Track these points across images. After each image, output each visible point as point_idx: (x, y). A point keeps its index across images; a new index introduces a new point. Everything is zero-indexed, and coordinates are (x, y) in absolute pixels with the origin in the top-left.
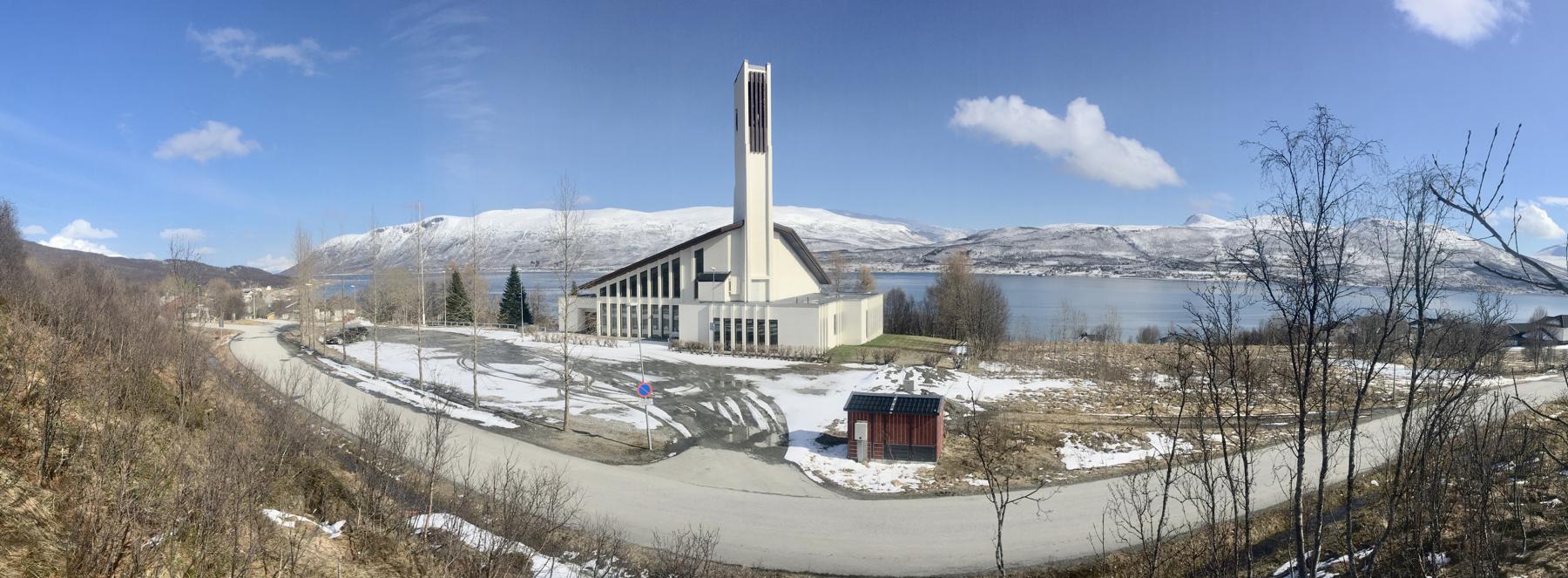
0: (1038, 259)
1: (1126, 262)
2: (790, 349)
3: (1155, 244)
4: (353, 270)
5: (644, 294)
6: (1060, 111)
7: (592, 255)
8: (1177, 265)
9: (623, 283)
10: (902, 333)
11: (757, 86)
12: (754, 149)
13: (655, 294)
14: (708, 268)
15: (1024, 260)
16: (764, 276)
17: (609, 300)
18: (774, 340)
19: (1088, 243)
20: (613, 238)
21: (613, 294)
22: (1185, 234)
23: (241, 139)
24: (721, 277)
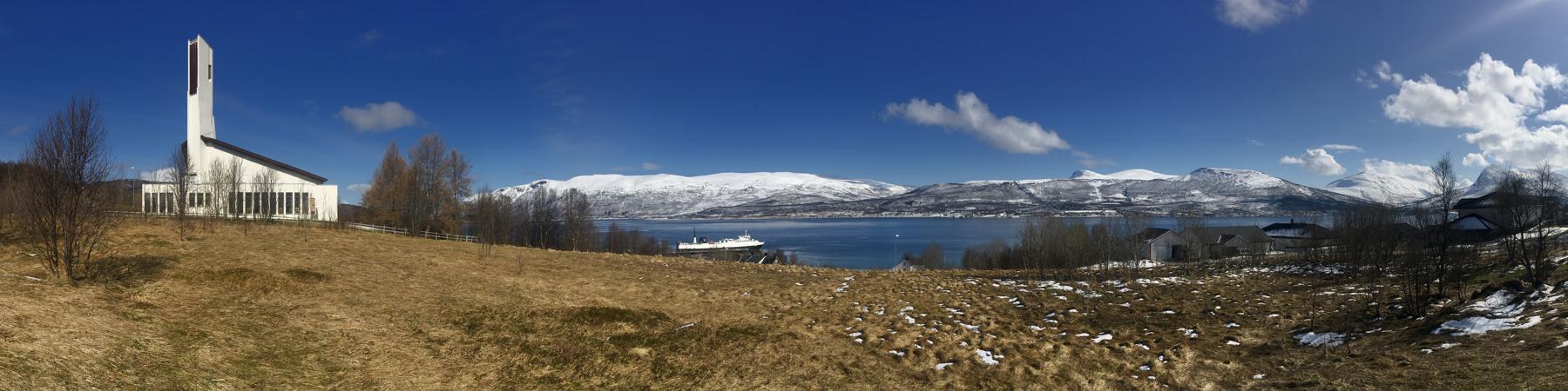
1: (1023, 205)
3: (1046, 192)
4: (818, 210)
6: (951, 104)
7: (648, 207)
10: (534, 243)
15: (951, 207)
20: (664, 195)
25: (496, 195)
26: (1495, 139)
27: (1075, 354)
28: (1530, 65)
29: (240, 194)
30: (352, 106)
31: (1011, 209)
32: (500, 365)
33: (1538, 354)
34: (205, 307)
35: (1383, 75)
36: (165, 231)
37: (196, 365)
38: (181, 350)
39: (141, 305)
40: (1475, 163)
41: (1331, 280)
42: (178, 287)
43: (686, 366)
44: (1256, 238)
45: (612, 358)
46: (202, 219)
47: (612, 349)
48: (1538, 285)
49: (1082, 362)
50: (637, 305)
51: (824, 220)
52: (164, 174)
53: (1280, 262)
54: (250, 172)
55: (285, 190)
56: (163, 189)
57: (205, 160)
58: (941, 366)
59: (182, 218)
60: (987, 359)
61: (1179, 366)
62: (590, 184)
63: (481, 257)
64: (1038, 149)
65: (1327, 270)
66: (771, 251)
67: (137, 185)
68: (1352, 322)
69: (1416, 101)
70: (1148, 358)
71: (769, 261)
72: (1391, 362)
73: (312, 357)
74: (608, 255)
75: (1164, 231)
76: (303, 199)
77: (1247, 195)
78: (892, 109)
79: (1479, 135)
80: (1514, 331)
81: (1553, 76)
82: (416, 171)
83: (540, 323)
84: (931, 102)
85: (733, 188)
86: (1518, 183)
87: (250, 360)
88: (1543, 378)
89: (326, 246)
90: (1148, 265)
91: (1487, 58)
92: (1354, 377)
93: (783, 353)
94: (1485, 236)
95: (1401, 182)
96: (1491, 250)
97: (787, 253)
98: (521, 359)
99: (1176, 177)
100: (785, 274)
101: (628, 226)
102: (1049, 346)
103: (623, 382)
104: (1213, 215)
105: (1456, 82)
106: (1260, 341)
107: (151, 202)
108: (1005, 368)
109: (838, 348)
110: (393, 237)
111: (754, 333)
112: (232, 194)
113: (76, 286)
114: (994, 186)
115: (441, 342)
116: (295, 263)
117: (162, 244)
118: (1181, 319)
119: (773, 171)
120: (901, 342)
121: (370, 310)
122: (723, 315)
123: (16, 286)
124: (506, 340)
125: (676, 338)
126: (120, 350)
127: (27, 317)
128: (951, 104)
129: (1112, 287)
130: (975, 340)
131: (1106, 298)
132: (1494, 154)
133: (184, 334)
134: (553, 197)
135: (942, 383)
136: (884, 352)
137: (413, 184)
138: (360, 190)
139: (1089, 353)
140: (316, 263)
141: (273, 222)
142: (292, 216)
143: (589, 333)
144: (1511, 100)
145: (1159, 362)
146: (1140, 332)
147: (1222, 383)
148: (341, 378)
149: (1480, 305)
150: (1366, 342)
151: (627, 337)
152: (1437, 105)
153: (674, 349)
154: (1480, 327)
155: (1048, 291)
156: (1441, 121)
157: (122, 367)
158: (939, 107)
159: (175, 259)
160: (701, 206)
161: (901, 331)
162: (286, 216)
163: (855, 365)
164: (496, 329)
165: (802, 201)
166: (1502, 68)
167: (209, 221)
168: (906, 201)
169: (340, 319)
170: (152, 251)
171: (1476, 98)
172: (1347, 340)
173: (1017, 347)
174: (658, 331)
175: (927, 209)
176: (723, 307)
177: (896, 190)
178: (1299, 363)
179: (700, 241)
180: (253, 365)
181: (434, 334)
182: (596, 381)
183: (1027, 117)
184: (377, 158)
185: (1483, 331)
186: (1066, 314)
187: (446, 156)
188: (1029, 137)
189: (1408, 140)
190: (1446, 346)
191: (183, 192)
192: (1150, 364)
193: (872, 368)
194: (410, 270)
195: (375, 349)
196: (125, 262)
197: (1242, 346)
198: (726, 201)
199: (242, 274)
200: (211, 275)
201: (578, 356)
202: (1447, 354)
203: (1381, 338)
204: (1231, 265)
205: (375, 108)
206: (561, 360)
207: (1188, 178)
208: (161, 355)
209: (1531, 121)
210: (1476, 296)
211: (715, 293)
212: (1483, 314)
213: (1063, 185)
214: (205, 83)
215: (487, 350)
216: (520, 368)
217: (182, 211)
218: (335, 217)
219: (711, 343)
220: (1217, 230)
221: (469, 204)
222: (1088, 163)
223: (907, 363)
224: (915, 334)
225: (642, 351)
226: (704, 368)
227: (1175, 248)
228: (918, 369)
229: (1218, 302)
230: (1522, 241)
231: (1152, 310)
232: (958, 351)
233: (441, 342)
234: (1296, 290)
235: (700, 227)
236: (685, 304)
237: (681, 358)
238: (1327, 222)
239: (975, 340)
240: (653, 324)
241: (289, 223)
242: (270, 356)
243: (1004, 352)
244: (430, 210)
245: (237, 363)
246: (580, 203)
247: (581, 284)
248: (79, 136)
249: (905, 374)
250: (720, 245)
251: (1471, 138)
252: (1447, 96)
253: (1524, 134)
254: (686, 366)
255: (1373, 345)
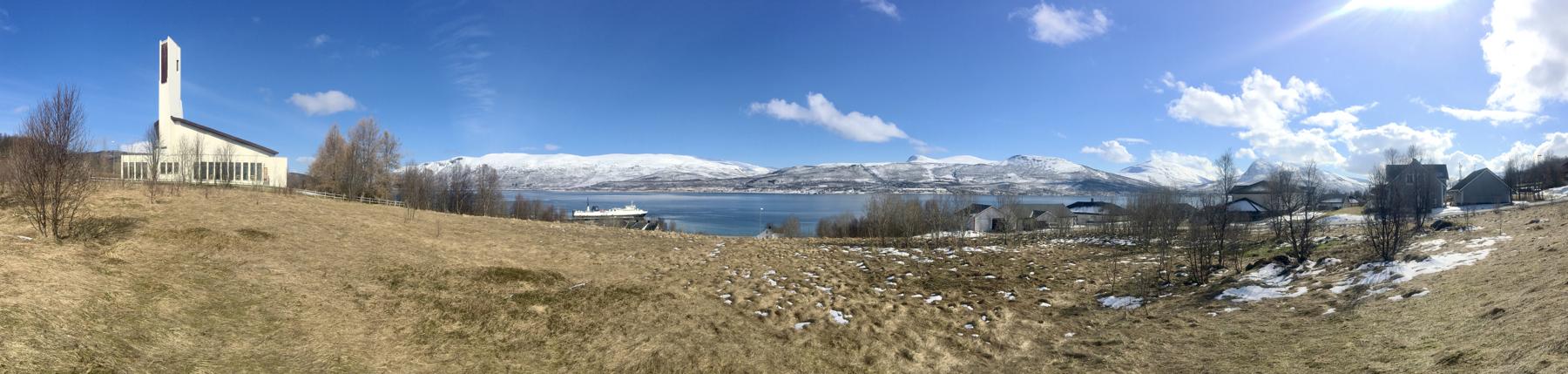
0: (816, 184)
3: (887, 173)
6: (804, 104)
8: (901, 185)
10: (452, 209)
19: (846, 174)
20: (562, 171)
22: (908, 166)
25: (421, 168)
26: (1263, 137)
27: (911, 313)
28: (1293, 80)
29: (203, 164)
30: (302, 93)
31: (857, 187)
32: (416, 320)
33: (1307, 319)
34: (168, 263)
35: (1169, 84)
36: (139, 194)
37: (156, 315)
38: (143, 301)
39: (113, 261)
40: (1246, 156)
41: (1125, 251)
42: (147, 244)
43: (577, 323)
44: (1063, 213)
45: (514, 314)
46: (171, 184)
47: (514, 306)
48: (1302, 260)
49: (917, 323)
50: (537, 266)
51: (700, 194)
52: (142, 146)
53: (1083, 234)
54: (212, 148)
55: (242, 160)
56: (139, 159)
57: (174, 138)
58: (800, 326)
59: (154, 185)
60: (838, 318)
61: (1000, 326)
62: (499, 161)
63: (406, 220)
64: (880, 139)
65: (1122, 242)
66: (651, 221)
67: (115, 157)
68: (1150, 288)
69: (1196, 104)
70: (972, 318)
71: (652, 227)
72: (1183, 323)
73: (255, 307)
74: (514, 220)
75: (985, 207)
76: (257, 169)
77: (1055, 180)
78: (756, 107)
79: (1250, 134)
80: (1285, 299)
81: (1314, 89)
82: (354, 147)
83: (453, 281)
84: (789, 102)
85: (621, 166)
86: (1285, 175)
87: (203, 310)
88: (1313, 340)
89: (274, 208)
90: (973, 235)
91: (1259, 73)
92: (1153, 336)
93: (662, 311)
94: (1255, 217)
95: (1185, 170)
96: (1261, 228)
97: (668, 222)
98: (433, 315)
99: (996, 163)
100: (665, 239)
101: (530, 196)
102: (890, 306)
103: (522, 337)
104: (1025, 194)
105: (1233, 91)
106: (1069, 304)
107: (129, 172)
108: (854, 327)
109: (709, 308)
110: (333, 202)
111: (634, 292)
112: (196, 166)
113: (60, 243)
114: (843, 168)
115: (367, 297)
116: (246, 223)
117: (134, 206)
118: (1000, 282)
119: (655, 152)
120: (764, 303)
121: (306, 267)
122: (610, 275)
123: (11, 245)
124: (422, 296)
125: (571, 297)
126: (92, 302)
127: (14, 274)
128: (804, 104)
129: (942, 254)
130: (828, 301)
131: (937, 264)
132: (1262, 149)
133: (147, 286)
134: (468, 171)
135: (801, 342)
136: (750, 312)
137: (350, 157)
138: (305, 164)
139: (922, 313)
140: (263, 223)
141: (231, 187)
142: (249, 182)
143: (495, 291)
144: (1280, 107)
145: (982, 322)
146: (965, 294)
147: (1037, 341)
148: (276, 327)
149: (1254, 275)
150: (1161, 305)
151: (527, 295)
152: (1222, 112)
153: (567, 306)
154: (1255, 294)
155: (889, 257)
156: (1218, 121)
157: (94, 317)
158: (794, 105)
159: (145, 220)
160: (593, 181)
161: (764, 293)
162: (242, 182)
163: (725, 325)
164: (414, 286)
165: (682, 178)
166: (1270, 81)
167: (181, 184)
168: (770, 180)
169: (278, 272)
170: (126, 213)
171: (1253, 104)
172: (1143, 305)
173: (863, 307)
174: (554, 290)
175: (787, 187)
176: (611, 268)
177: (761, 171)
178: (1104, 323)
179: (593, 209)
180: (205, 314)
181: (361, 289)
182: (499, 336)
183: (868, 112)
184: (321, 137)
185: (1258, 298)
186: (903, 277)
187: (380, 136)
188: (867, 128)
189: (1194, 135)
190: (1228, 310)
191: (155, 162)
192: (973, 323)
193: (740, 328)
194: (345, 231)
195: (307, 302)
196: (101, 222)
197: (1054, 308)
198: (615, 177)
199: (200, 232)
200: (175, 234)
201: (483, 313)
202: (1231, 317)
203: (1172, 302)
204: (1042, 235)
205: (321, 96)
206: (469, 315)
207: (1005, 163)
208: (128, 305)
209: (1295, 124)
210: (1250, 268)
211: (604, 256)
212: (1257, 284)
213: (902, 168)
214: (174, 73)
215: (407, 305)
216: (433, 323)
217: (154, 177)
218: (284, 184)
219: (600, 301)
220: (1030, 206)
221: (398, 175)
222: (923, 150)
223: (770, 322)
224: (777, 296)
225: (540, 309)
226: (592, 325)
227: (995, 221)
228: (779, 328)
229: (1032, 269)
230: (1291, 222)
231: (976, 274)
232: (814, 311)
233: (367, 297)
234: (1097, 259)
235: (592, 198)
236: (578, 266)
237: (573, 315)
238: (1122, 201)
239: (828, 301)
240: (549, 283)
241: (245, 188)
242: (219, 307)
243: (853, 312)
244: (365, 179)
245: (191, 313)
246: (491, 177)
247: (489, 246)
248: (64, 114)
249: (769, 334)
250: (609, 213)
251: (1242, 135)
252: (1224, 101)
253: (1288, 135)
254: (577, 323)
255: (1166, 307)
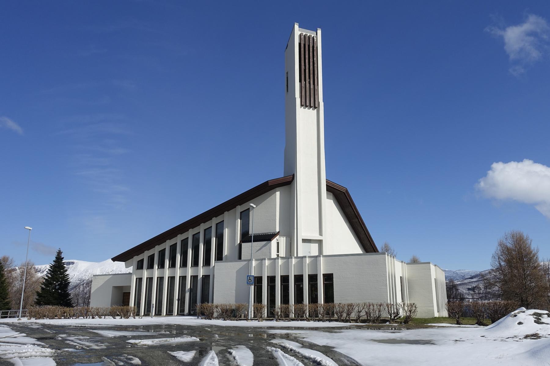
2: (351, 306)
5: (184, 264)
9: (162, 254)
11: (307, 47)
12: (304, 105)
13: (195, 263)
14: (254, 230)
16: (317, 237)
17: (145, 274)
18: (329, 297)
21: (151, 266)
23: (127, 267)
24: (268, 238)
